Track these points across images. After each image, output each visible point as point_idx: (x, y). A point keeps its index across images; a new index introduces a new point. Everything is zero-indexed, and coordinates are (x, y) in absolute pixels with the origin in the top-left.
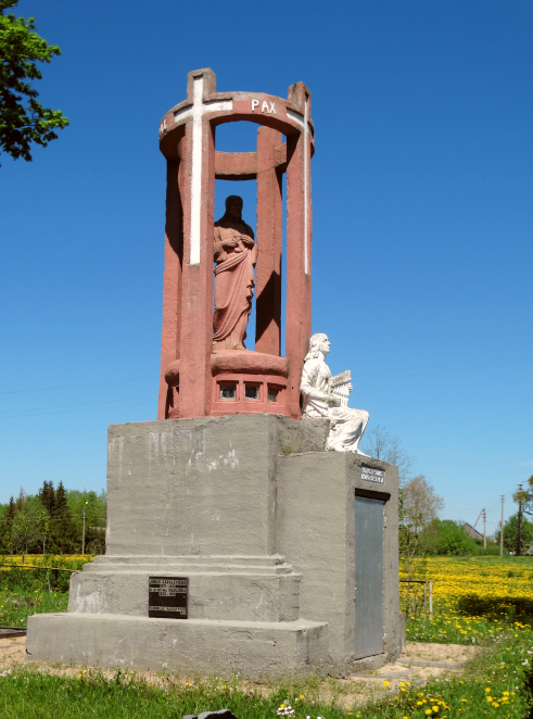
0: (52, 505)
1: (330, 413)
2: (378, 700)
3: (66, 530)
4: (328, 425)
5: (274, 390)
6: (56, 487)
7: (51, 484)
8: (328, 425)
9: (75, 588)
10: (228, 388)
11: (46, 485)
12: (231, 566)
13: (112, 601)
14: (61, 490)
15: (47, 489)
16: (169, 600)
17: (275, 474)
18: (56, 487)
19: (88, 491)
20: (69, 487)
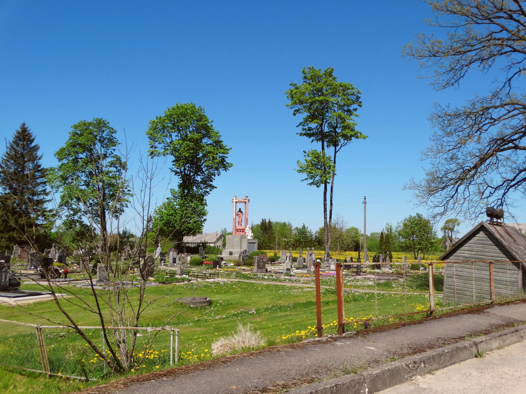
0: (266, 229)
1: (248, 234)
2: (496, 341)
3: (270, 240)
4: (248, 236)
5: (243, 231)
6: (267, 221)
7: (265, 220)
8: (248, 236)
9: (223, 253)
10: (238, 231)
11: (263, 220)
12: (488, 254)
13: (226, 254)
14: (270, 222)
15: (263, 223)
16: (231, 253)
17: (241, 241)
18: (267, 221)
19: (283, 222)
20: (273, 220)
